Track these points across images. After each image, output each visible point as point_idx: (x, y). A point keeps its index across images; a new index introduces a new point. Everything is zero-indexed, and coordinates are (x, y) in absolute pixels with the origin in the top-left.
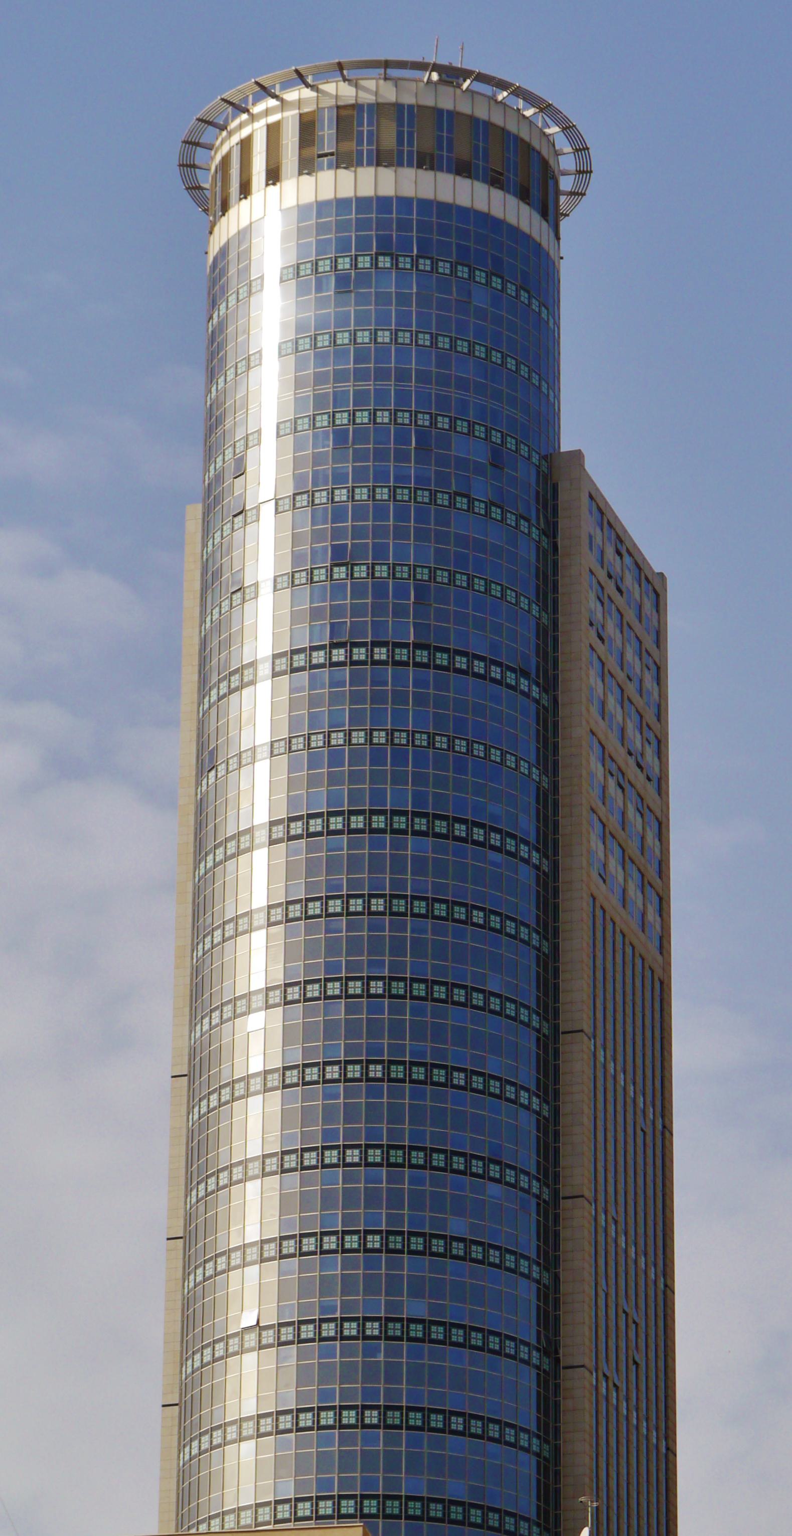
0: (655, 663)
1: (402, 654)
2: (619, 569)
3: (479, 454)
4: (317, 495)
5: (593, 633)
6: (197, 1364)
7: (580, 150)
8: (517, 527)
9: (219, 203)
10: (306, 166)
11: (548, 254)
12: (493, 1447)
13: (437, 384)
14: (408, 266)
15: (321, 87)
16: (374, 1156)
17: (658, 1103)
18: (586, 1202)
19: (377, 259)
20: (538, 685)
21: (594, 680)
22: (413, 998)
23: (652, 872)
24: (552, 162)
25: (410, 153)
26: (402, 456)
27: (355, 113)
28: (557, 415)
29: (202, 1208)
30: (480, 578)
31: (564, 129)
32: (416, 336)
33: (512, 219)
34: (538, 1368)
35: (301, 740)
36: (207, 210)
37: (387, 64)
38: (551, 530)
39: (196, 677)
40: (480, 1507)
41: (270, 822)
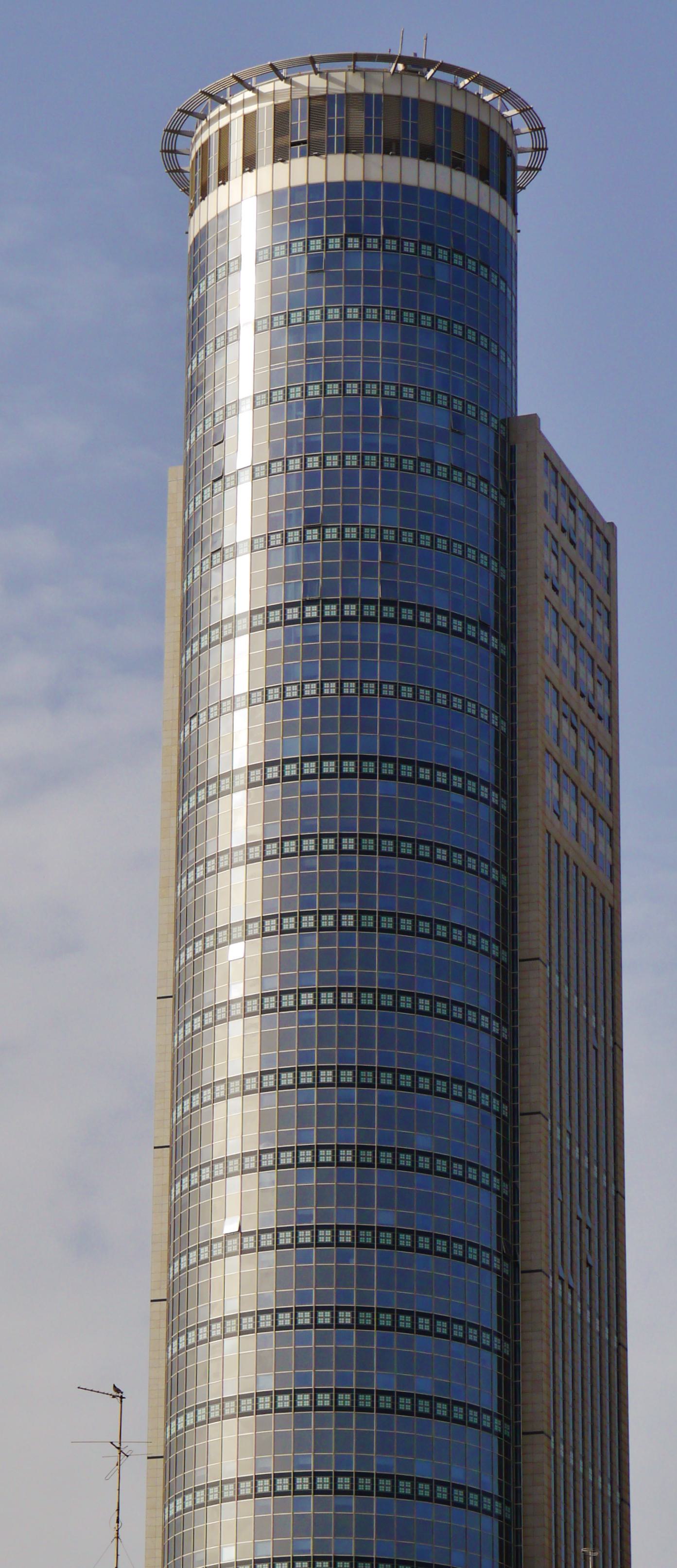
0: (606, 609)
1: (370, 611)
2: (572, 522)
3: (441, 420)
4: (291, 462)
5: (549, 586)
6: (187, 1108)
7: (536, 129)
8: (477, 488)
9: (199, 187)
10: (281, 154)
11: (506, 230)
12: (455, 797)
13: (402, 357)
14: (376, 246)
15: (294, 79)
16: (350, 610)
17: (609, 1022)
18: (542, 1118)
19: (346, 240)
20: (496, 636)
21: (549, 629)
22: (381, 930)
23: (603, 806)
24: (510, 142)
25: (378, 140)
26: (370, 425)
27: (326, 103)
28: (514, 380)
29: (191, 894)
30: (443, 538)
31: (521, 112)
32: (383, 312)
33: (472, 199)
34: (498, 1272)
35: (277, 690)
36: (188, 190)
37: (356, 57)
38: (508, 490)
39: (178, 628)
40: (446, 1401)
41: (248, 766)
